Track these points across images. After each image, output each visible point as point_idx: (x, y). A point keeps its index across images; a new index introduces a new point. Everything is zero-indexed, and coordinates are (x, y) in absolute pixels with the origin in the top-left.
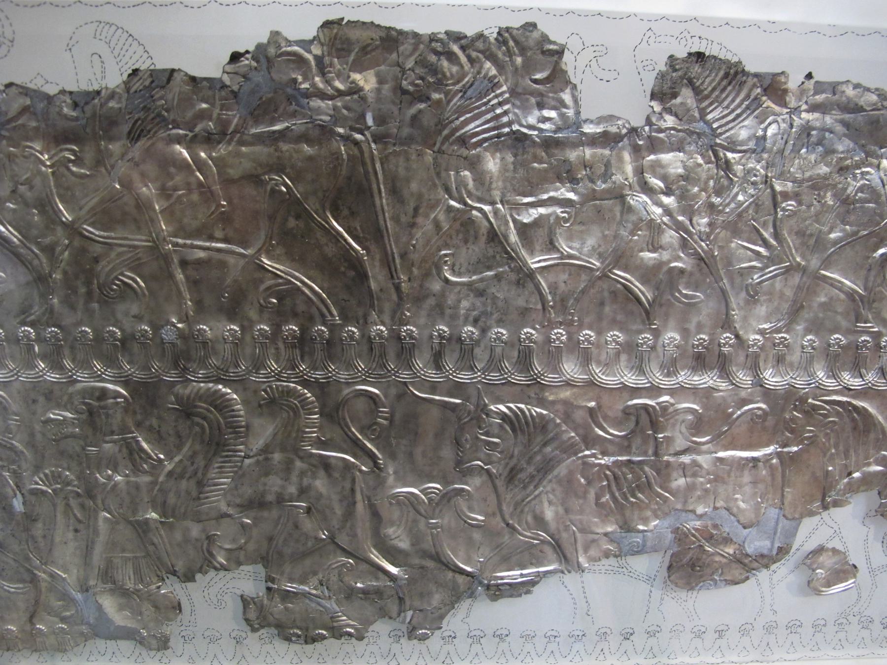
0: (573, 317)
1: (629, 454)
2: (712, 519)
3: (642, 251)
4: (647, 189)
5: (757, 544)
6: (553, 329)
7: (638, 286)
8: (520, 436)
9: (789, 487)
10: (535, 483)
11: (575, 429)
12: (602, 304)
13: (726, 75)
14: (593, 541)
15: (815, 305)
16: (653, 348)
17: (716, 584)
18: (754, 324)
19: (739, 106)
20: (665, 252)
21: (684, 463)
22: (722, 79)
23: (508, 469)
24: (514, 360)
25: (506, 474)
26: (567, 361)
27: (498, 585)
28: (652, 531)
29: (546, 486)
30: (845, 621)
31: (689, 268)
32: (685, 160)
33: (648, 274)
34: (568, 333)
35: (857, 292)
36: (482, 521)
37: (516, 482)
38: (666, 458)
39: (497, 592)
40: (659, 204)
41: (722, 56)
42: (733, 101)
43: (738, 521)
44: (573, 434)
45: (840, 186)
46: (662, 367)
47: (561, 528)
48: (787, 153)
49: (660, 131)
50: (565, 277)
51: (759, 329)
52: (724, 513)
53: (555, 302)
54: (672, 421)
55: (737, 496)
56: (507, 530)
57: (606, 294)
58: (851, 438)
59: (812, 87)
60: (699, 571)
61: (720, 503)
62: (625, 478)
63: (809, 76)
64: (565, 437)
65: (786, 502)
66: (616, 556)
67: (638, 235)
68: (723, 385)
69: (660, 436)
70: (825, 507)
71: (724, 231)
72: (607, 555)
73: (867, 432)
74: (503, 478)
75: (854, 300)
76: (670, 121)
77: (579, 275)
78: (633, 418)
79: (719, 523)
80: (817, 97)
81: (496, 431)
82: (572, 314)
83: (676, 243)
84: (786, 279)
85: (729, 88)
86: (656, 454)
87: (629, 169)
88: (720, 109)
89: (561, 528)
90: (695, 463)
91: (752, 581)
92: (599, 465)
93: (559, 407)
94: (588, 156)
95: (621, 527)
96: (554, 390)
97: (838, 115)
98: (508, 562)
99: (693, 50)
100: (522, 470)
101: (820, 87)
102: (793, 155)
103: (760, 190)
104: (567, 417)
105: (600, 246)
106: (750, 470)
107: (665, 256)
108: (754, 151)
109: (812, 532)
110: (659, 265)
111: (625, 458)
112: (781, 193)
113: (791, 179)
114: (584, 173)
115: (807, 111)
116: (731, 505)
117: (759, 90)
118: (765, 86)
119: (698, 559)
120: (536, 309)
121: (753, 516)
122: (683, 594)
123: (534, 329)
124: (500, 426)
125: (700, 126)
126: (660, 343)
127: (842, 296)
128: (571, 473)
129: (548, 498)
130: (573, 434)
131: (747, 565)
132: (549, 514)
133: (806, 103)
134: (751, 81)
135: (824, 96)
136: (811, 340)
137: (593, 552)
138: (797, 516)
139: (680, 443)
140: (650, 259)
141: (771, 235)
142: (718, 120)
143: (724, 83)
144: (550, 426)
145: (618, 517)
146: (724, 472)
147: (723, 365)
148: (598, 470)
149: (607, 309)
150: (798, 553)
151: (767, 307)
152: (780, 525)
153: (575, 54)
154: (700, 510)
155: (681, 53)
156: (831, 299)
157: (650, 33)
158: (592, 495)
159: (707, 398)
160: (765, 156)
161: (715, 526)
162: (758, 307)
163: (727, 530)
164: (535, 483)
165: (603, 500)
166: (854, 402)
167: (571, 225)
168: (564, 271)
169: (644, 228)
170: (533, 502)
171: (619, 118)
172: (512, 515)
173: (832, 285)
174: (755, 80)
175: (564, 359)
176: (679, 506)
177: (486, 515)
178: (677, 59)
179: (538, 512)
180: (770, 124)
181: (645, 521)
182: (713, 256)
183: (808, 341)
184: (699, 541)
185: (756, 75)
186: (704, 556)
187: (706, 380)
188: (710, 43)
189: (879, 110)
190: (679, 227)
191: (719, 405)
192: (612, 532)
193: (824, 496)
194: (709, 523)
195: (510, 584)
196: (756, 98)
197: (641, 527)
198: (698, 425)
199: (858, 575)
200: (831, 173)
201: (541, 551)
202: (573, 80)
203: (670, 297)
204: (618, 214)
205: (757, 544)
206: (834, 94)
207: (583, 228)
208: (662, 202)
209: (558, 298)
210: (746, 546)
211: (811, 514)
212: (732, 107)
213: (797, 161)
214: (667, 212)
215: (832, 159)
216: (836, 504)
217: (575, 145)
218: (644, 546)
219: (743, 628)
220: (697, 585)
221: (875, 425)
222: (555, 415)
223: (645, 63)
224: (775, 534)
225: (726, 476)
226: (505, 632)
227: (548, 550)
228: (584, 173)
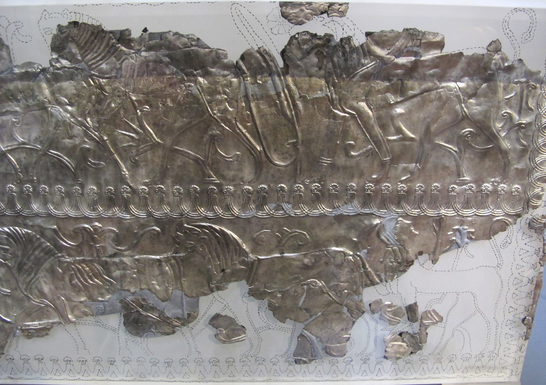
0: (33, 177)
1: (83, 256)
2: (140, 295)
3: (64, 138)
4: (60, 104)
5: (174, 311)
6: (24, 184)
7: (66, 159)
8: (19, 246)
9: (184, 277)
10: (34, 271)
11: (49, 242)
12: (48, 170)
13: (93, 33)
14: (75, 306)
15: (175, 167)
16: (82, 194)
17: (154, 334)
18: (140, 179)
19: (102, 51)
20: (76, 139)
21: (116, 262)
22: (91, 36)
23: (17, 263)
24: (6, 202)
25: (16, 266)
26: (35, 203)
27: (28, 330)
28: (107, 301)
29: (41, 274)
30: (247, 360)
31: (92, 147)
32: (75, 85)
33: (70, 152)
34: (32, 187)
35: (199, 159)
36: (9, 293)
37: (24, 271)
38: (104, 259)
39: (29, 334)
40: (67, 111)
41: (90, 23)
42: (99, 48)
43: (158, 297)
44: (49, 244)
45: (174, 95)
46: (89, 206)
47: (55, 298)
48: (135, 77)
49: (58, 69)
50: (24, 155)
51: (144, 183)
52: (147, 292)
53: (21, 169)
54: (103, 237)
55: (154, 282)
56: (26, 298)
57: (49, 164)
58: (219, 248)
59: (147, 37)
60: (141, 326)
61: (144, 286)
62: (85, 270)
63: (145, 30)
64: (44, 246)
65: (184, 287)
66: (93, 315)
67: (60, 130)
68: (128, 217)
69: (98, 245)
70: (212, 291)
71: (108, 126)
72: (86, 314)
73: (227, 245)
74: (15, 268)
75: (199, 164)
76: (65, 62)
77: (32, 154)
78: (80, 235)
79: (146, 297)
80: (150, 42)
81: (5, 242)
82: (32, 176)
83: (81, 133)
84: (154, 152)
85: (96, 41)
86: (98, 256)
87: (47, 92)
88: (92, 54)
89: (55, 298)
90: (122, 262)
91: (178, 333)
92: (67, 262)
93: (36, 228)
94: (20, 87)
95: (88, 298)
96: (32, 219)
97: (164, 51)
98: (29, 315)
99: (72, 20)
100: (25, 264)
101: (152, 36)
102: (139, 78)
103: (123, 99)
104: (43, 235)
105: (40, 137)
106: (158, 267)
107: (77, 141)
108: (116, 77)
109: (209, 305)
110: (75, 147)
111: (81, 258)
112: (136, 101)
113: (141, 92)
114: (21, 96)
115: (145, 51)
116: (151, 287)
117: (114, 41)
118: (117, 38)
119: (138, 319)
120: (11, 174)
121: (165, 295)
122: (138, 339)
123: (13, 185)
124: (7, 239)
125: (83, 65)
126: (85, 191)
127: (191, 161)
128: (52, 266)
129: (44, 280)
130: (49, 244)
131: (167, 326)
132: (46, 289)
133: (144, 46)
134: (107, 36)
135: (154, 41)
136: (420, 186)
137: (76, 312)
138: (194, 295)
139: (111, 250)
140: (69, 143)
141: (137, 126)
142: (91, 60)
143: (92, 38)
144: (34, 240)
145: (86, 292)
146: (142, 268)
147: (125, 206)
148: (67, 265)
149: (51, 173)
150: (204, 318)
151: (146, 169)
152: (184, 301)
153: (5, 28)
154: (132, 290)
155: (65, 23)
156: (184, 163)
157: (45, 13)
158: (67, 279)
159: (120, 224)
160: (123, 79)
161: (144, 300)
162: (140, 170)
163: (152, 302)
164: (34, 271)
165: (74, 282)
166: (214, 226)
167: (21, 125)
168: (23, 152)
169: (62, 125)
170: (36, 283)
171: (34, 64)
172: (26, 290)
173: (182, 155)
174: (111, 35)
175: (33, 201)
176: (119, 287)
177: (11, 289)
178: (63, 27)
179: (39, 288)
180: (123, 61)
181: (102, 295)
182: (104, 140)
183: (418, 187)
184: (136, 308)
185: (111, 32)
186: (141, 317)
187: (117, 212)
188: (81, 15)
189: (190, 47)
190: (82, 124)
191: (128, 228)
192: (84, 301)
193: (211, 284)
194: (140, 298)
195: (34, 329)
196: (113, 46)
197: (100, 299)
198: (118, 240)
199: (247, 331)
200: (165, 87)
201: (47, 311)
202: (6, 43)
203: (85, 165)
204: (46, 118)
205: (174, 311)
206: (161, 39)
207: (29, 127)
208: (68, 110)
209: (22, 167)
210: (166, 311)
211: (205, 294)
212: (99, 52)
213: (142, 82)
214: (73, 116)
215: (164, 79)
216: (219, 289)
217: (12, 81)
218: (105, 310)
219: (181, 361)
220: (143, 334)
221: (230, 240)
222: (36, 233)
223: (46, 30)
224: (183, 306)
225: (143, 270)
226: (41, 357)
227: (53, 312)
228: (21, 96)
